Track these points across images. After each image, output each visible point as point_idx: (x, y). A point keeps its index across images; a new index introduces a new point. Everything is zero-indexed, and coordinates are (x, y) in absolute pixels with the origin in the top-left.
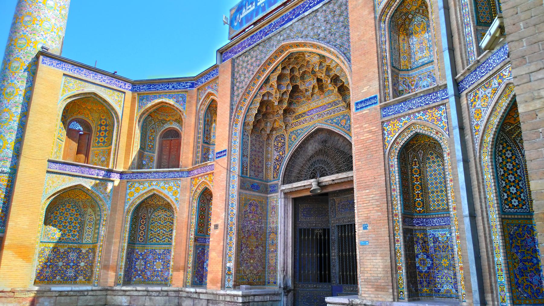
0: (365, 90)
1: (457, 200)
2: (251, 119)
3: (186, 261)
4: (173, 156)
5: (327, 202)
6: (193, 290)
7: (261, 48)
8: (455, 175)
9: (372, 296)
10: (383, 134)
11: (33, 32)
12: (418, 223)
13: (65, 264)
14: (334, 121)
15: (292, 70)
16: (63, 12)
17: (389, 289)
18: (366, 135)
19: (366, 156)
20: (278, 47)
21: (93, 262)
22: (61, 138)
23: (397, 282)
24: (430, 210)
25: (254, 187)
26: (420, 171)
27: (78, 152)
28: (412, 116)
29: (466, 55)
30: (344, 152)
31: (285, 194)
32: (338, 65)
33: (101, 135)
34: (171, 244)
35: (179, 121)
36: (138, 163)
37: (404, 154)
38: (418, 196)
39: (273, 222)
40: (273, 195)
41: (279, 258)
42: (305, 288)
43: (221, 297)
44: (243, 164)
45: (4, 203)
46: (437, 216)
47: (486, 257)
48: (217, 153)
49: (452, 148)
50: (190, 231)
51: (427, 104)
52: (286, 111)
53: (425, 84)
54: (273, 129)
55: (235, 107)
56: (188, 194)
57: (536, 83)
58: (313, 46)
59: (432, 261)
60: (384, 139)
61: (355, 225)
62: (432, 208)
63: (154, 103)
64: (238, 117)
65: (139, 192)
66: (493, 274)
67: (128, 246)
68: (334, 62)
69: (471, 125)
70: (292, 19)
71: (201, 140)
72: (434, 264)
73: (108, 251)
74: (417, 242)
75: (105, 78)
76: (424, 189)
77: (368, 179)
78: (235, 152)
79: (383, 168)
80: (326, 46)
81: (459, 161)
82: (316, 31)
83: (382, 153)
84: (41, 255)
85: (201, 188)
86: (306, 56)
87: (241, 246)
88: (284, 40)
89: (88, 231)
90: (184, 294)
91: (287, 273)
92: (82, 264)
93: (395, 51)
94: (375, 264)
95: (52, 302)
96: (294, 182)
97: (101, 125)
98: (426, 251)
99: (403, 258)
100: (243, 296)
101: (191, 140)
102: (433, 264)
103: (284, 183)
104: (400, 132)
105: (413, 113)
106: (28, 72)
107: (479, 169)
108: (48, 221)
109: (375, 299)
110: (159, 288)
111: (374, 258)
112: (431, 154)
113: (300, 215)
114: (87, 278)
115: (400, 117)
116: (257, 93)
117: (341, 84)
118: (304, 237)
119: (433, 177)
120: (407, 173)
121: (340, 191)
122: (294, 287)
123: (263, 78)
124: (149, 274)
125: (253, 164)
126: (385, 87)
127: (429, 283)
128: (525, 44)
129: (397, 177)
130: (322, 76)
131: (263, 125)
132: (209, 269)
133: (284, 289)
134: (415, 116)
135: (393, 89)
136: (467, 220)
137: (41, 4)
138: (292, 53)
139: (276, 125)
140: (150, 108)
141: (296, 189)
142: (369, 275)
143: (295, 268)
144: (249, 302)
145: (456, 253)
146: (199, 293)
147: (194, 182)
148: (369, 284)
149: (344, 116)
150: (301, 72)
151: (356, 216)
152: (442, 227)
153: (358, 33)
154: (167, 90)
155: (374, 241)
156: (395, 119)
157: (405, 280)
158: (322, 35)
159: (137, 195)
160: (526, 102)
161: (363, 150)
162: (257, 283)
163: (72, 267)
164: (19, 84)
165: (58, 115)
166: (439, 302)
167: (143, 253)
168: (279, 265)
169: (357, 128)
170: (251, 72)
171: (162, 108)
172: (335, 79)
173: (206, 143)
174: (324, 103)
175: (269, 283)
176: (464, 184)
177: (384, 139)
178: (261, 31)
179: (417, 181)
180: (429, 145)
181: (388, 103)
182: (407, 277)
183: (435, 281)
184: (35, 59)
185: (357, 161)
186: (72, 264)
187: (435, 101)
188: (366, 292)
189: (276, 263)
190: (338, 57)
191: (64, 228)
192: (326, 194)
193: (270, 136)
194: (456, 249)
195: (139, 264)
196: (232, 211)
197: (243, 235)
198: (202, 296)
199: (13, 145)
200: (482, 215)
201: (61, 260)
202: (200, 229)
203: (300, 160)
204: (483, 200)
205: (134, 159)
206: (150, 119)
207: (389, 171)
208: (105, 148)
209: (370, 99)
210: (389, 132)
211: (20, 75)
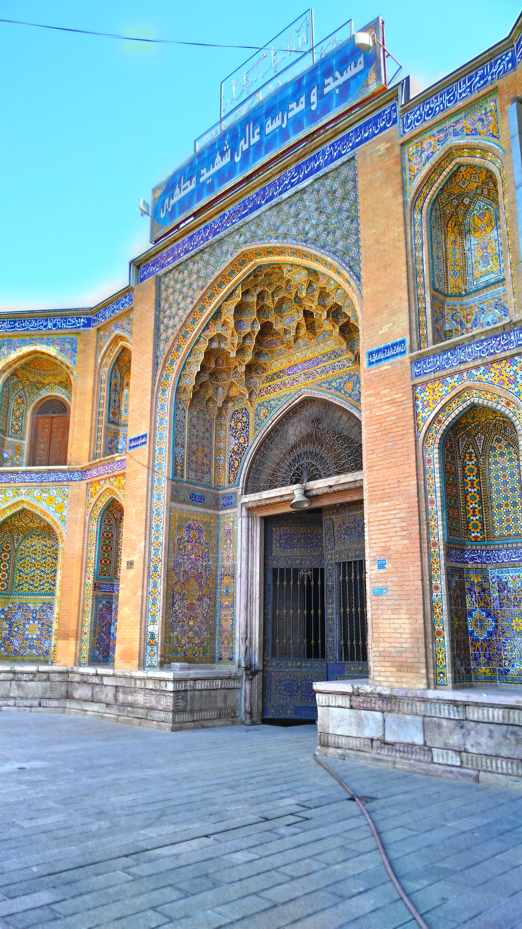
0: (385, 329)
2: (190, 382)
3: (80, 623)
5: (320, 523)
6: (91, 670)
7: (206, 256)
9: (392, 679)
10: (415, 406)
12: (473, 559)
14: (334, 384)
15: (261, 296)
17: (419, 668)
19: (384, 445)
20: (235, 255)
23: (435, 657)
25: (196, 499)
26: (478, 470)
28: (465, 374)
30: (349, 438)
31: (249, 509)
32: (338, 287)
34: (53, 594)
35: (66, 385)
37: (450, 440)
40: (228, 511)
41: (237, 618)
42: (281, 667)
44: (175, 458)
48: (131, 441)
51: (491, 354)
52: (250, 368)
53: (490, 320)
56: (82, 510)
58: (296, 252)
59: (496, 621)
60: (416, 415)
62: (497, 533)
63: (21, 354)
68: (332, 282)
71: (103, 418)
72: (500, 627)
74: (470, 590)
76: (485, 500)
77: (387, 483)
78: (161, 438)
79: (414, 465)
80: (318, 254)
82: (301, 227)
85: (105, 500)
86: (285, 270)
87: (173, 598)
88: (245, 242)
90: (77, 678)
91: (251, 643)
94: (397, 626)
96: (264, 490)
99: (445, 617)
100: (176, 681)
101: (87, 418)
102: (496, 627)
103: (246, 491)
104: (443, 402)
105: (467, 370)
109: (396, 685)
110: (32, 668)
112: (498, 441)
113: (274, 546)
115: (444, 377)
116: (200, 336)
117: (345, 320)
118: (282, 581)
120: (455, 474)
121: (341, 504)
122: (264, 666)
123: (210, 309)
124: (17, 645)
125: (194, 458)
126: (419, 325)
129: (438, 480)
130: (313, 306)
131: (211, 392)
132: (118, 635)
133: (246, 669)
135: (434, 328)
138: (260, 267)
139: (234, 392)
140: (15, 361)
141: (268, 502)
144: (185, 691)
146: (102, 676)
147: (92, 490)
148: (387, 659)
149: (351, 376)
150: (277, 299)
151: (367, 546)
153: (374, 231)
156: (435, 379)
157: (448, 654)
158: (312, 234)
161: (380, 434)
162: (200, 658)
169: (370, 396)
170: (189, 300)
172: (335, 312)
173: (113, 422)
174: (316, 354)
175: (220, 659)
177: (416, 415)
178: (206, 227)
179: (472, 487)
180: (495, 424)
181: (424, 353)
182: (452, 649)
183: (500, 655)
185: (370, 452)
187: (506, 348)
188: (382, 674)
189: (233, 625)
190: (339, 273)
192: (319, 510)
193: (224, 411)
196: (157, 538)
198: (106, 681)
202: (103, 568)
203: (275, 451)
209: (393, 345)
210: (425, 403)
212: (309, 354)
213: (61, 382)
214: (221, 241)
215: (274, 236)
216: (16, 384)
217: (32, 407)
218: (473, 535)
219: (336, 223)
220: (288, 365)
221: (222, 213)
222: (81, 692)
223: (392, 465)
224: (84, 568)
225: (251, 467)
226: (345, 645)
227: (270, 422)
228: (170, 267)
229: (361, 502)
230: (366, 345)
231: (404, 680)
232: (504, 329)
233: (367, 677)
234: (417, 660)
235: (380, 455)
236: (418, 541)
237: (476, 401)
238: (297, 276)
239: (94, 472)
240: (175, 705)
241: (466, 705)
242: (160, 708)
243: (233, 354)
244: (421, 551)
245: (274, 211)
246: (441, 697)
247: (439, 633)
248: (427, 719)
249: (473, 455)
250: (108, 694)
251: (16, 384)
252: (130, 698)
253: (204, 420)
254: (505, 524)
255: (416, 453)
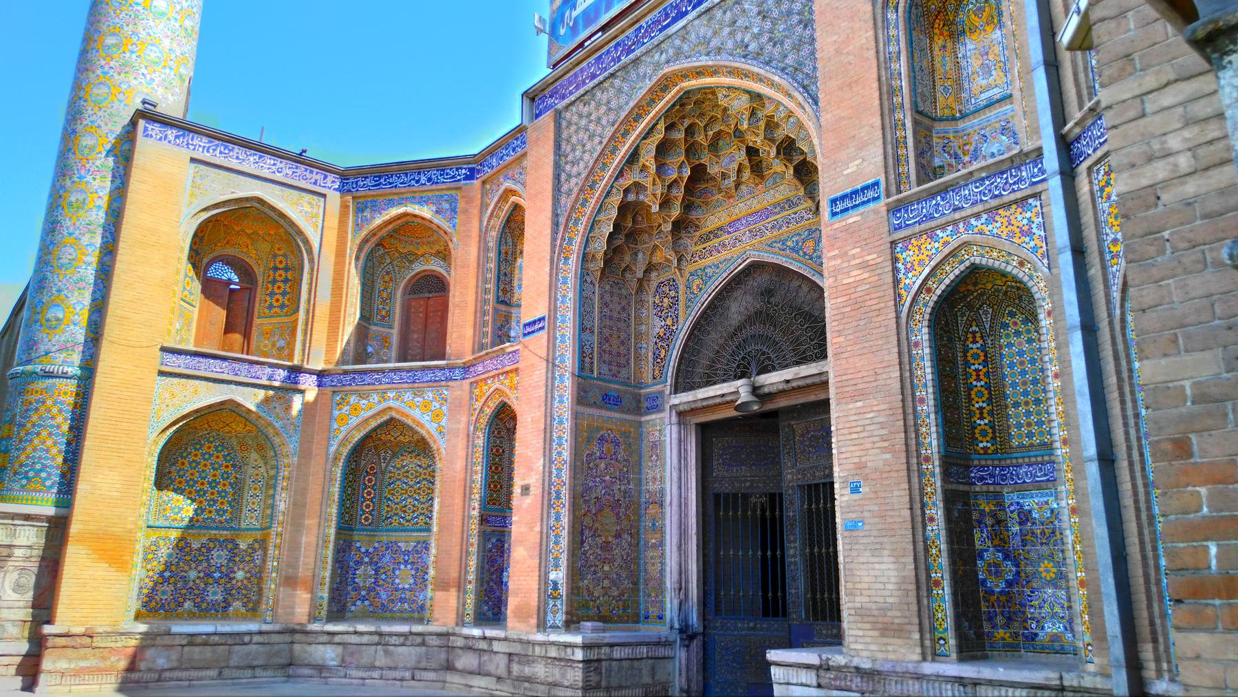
0: (852, 168)
1: (1070, 422)
2: (600, 246)
3: (463, 569)
4: (433, 335)
5: (776, 431)
6: (476, 632)
7: (617, 82)
8: (1065, 362)
9: (873, 647)
10: (895, 270)
11: (124, 68)
12: (982, 479)
13: (202, 575)
14: (789, 243)
15: (690, 131)
16: (188, 23)
17: (910, 632)
18: (855, 273)
19: (855, 323)
20: (655, 79)
21: (262, 569)
22: (190, 298)
23: (932, 616)
24: (1011, 447)
25: (610, 401)
26: (985, 356)
27: (229, 329)
28: (961, 225)
29: (1087, 76)
30: (811, 315)
31: (680, 414)
32: (790, 114)
33: (276, 291)
34: (429, 530)
35: (444, 255)
36: (356, 349)
37: (945, 315)
38: (981, 413)
39: (655, 479)
40: (653, 416)
41: (668, 561)
42: (728, 629)
43: (537, 649)
44: (582, 347)
45: (68, 444)
46: (1027, 460)
47: (1138, 557)
48: (525, 325)
49: (1056, 298)
50: (470, 499)
51: (996, 196)
52: (680, 226)
53: (995, 151)
54: (650, 268)
55: (562, 220)
56: (464, 419)
57: (1157, 118)
58: (733, 72)
59: (1017, 566)
60: (896, 282)
61: (832, 483)
62: (1015, 443)
63: (387, 217)
64: (571, 240)
65: (358, 414)
66: (1155, 597)
67: (338, 533)
68: (782, 108)
69: (1100, 241)
70: (686, 13)
71: (491, 297)
72: (1023, 574)
73: (295, 547)
74: (979, 522)
75: (280, 164)
76: (996, 397)
77: (860, 375)
78: (563, 321)
79: (896, 350)
80: (762, 72)
81: (1072, 328)
82: (739, 36)
83: (894, 315)
84: (150, 556)
85: (493, 404)
86: (720, 96)
87: (582, 534)
88: (668, 62)
89: (252, 502)
90: (460, 642)
91: (686, 595)
92: (240, 575)
93: (923, 75)
94: (878, 573)
95: (174, 657)
96: (700, 387)
97: (276, 269)
98: (1001, 543)
99: (944, 561)
100: (586, 647)
101: (471, 297)
102: (1018, 573)
103: (677, 389)
104: (933, 263)
105: (964, 219)
106: (116, 156)
107: (1121, 347)
108: (165, 481)
109: (880, 656)
110: (403, 628)
111: (876, 560)
112: (1012, 315)
113: (715, 463)
114: (251, 605)
115: (933, 229)
116: (612, 187)
117: (802, 158)
118: (726, 511)
119: (1017, 369)
120: (953, 362)
121: (803, 405)
122: (705, 627)
123: (624, 150)
124: (384, 597)
125: (606, 347)
126: (897, 160)
127: (1010, 619)
128: (1132, 26)
129: (929, 370)
130: (757, 140)
131: (627, 258)
132: (511, 585)
133: (681, 631)
134: (968, 226)
135: (917, 163)
136: (1093, 469)
137: (140, 8)
138: (688, 92)
139: (658, 258)
140: (380, 227)
141: (705, 403)
142: (867, 599)
143: (705, 583)
144: (599, 660)
145: (1070, 547)
146: (492, 639)
147: (477, 391)
148: (866, 619)
149: (811, 232)
150: (711, 133)
151: (835, 462)
152: (1039, 486)
153: (835, 38)
155: (877, 520)
156: (921, 233)
157: (949, 611)
158: (753, 46)
159: (354, 421)
160: (1133, 166)
161: (848, 309)
162: (619, 616)
163: (217, 582)
164: (96, 184)
165: (182, 249)
166: (1030, 663)
167: (371, 550)
168: (668, 576)
169: (834, 258)
170: (597, 140)
171: (407, 227)
172: (788, 148)
173: (503, 302)
174: (765, 204)
175: (647, 618)
176: (1086, 382)
177: (896, 282)
178: (618, 44)
179: (978, 379)
180: (1006, 292)
181: (906, 198)
182: (956, 605)
183: (1024, 613)
184: (130, 128)
185: (836, 334)
186: (217, 575)
187: (1015, 187)
188: (860, 640)
189: (662, 571)
190: (790, 96)
191: (200, 496)
192: (774, 414)
193: (645, 284)
194: (1069, 538)
195: (363, 576)
196: (559, 454)
197: (584, 508)
198: (497, 646)
199: (86, 316)
200: (1130, 456)
201: (193, 565)
202: (491, 495)
203: (713, 336)
204: (1132, 422)
205: (348, 343)
206: (382, 251)
207: (910, 356)
208: (286, 319)
209: (863, 189)
210: (909, 266)
211: (98, 163)
212: (756, 205)
213: (439, 252)
214: (636, 61)
215: (704, 52)
216: (382, 257)
217: (403, 285)
218: (981, 445)
219: (784, 30)
220: (728, 220)
221: (637, 26)
222: (466, 661)
223: (866, 351)
224: (467, 497)
225: (682, 358)
226: (814, 599)
227: (706, 296)
228: (573, 98)
229: (825, 404)
230: (827, 190)
231: (890, 648)
232: (1012, 162)
233: (841, 644)
234: (907, 621)
235: (850, 337)
236: (904, 454)
237: (977, 261)
238: (736, 102)
239: (480, 368)
240: (586, 680)
242: (566, 683)
243: (655, 208)
244: (908, 469)
245: (705, 18)
246: (941, 672)
247: (937, 584)
249: (978, 335)
250: (498, 664)
251: (382, 257)
252: (527, 670)
253: (620, 296)
254: (1024, 430)
255: (898, 334)
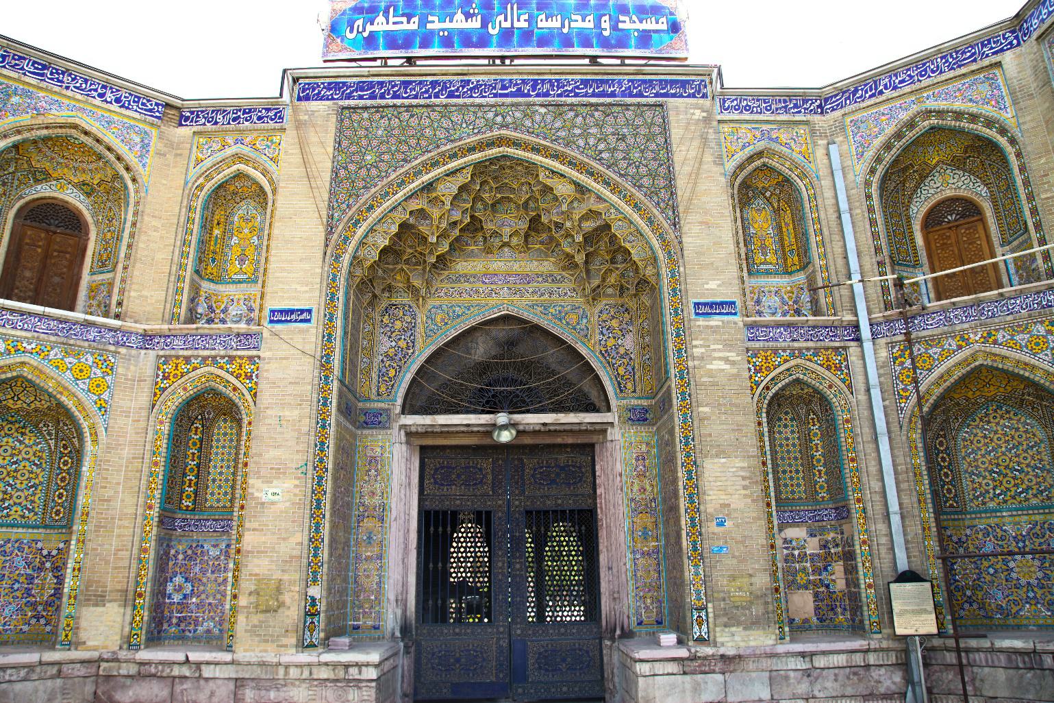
14: (551, 310)
70: (528, 95)
103: (408, 408)
109: (742, 644)
116: (400, 204)
146: (198, 665)
154: (98, 101)
198: (207, 672)
217: (17, 206)
241: (812, 654)
246: (791, 650)
248: (775, 673)
254: (789, 489)
